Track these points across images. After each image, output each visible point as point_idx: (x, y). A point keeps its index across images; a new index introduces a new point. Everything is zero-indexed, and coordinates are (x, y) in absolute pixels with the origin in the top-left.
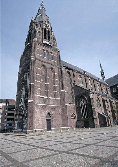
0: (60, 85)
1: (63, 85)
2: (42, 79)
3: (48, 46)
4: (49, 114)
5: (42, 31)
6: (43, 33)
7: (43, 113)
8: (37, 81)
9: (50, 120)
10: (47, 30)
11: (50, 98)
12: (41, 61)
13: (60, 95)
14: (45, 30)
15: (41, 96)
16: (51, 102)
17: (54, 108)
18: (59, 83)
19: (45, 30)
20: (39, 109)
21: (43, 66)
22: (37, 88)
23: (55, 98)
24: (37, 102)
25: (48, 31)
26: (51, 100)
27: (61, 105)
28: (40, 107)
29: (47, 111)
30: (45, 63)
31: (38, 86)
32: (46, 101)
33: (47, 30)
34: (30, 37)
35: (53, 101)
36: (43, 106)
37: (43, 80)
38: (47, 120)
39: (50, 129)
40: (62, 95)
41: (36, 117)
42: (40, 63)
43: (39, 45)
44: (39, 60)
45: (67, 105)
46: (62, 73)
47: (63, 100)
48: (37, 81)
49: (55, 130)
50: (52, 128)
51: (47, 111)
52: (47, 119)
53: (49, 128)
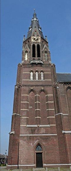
0: (55, 108)
1: (58, 107)
2: (31, 106)
3: (37, 64)
4: (39, 145)
5: (30, 49)
6: (32, 51)
7: (30, 145)
8: (23, 110)
9: (41, 153)
10: (36, 45)
11: (40, 126)
12: (29, 86)
13: (56, 120)
14: (34, 46)
15: (28, 126)
16: (43, 131)
17: (46, 138)
18: (54, 99)
19: (34, 46)
20: (25, 140)
21: (32, 90)
22: (23, 117)
23: (48, 126)
24: (22, 133)
25: (38, 46)
26: (42, 128)
27: (56, 124)
28: (26, 138)
29: (36, 142)
30: (34, 87)
31: (24, 115)
32: (35, 131)
33: (36, 45)
34: (18, 91)
35: (44, 129)
36: (30, 136)
37: (31, 107)
38: (37, 153)
39: (41, 166)
40: (59, 119)
41: (20, 150)
42: (27, 89)
43: (26, 68)
44: (25, 86)
45: (66, 132)
46: (57, 93)
47: (60, 127)
48: (23, 110)
49: (49, 167)
50: (44, 165)
51: (36, 142)
52: (36, 152)
53: (39, 163)
